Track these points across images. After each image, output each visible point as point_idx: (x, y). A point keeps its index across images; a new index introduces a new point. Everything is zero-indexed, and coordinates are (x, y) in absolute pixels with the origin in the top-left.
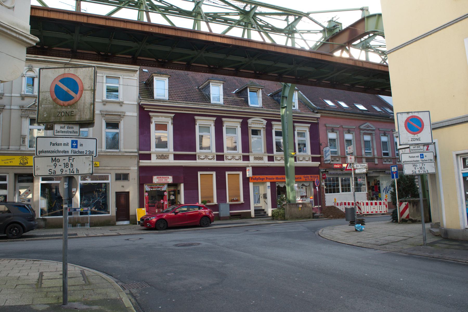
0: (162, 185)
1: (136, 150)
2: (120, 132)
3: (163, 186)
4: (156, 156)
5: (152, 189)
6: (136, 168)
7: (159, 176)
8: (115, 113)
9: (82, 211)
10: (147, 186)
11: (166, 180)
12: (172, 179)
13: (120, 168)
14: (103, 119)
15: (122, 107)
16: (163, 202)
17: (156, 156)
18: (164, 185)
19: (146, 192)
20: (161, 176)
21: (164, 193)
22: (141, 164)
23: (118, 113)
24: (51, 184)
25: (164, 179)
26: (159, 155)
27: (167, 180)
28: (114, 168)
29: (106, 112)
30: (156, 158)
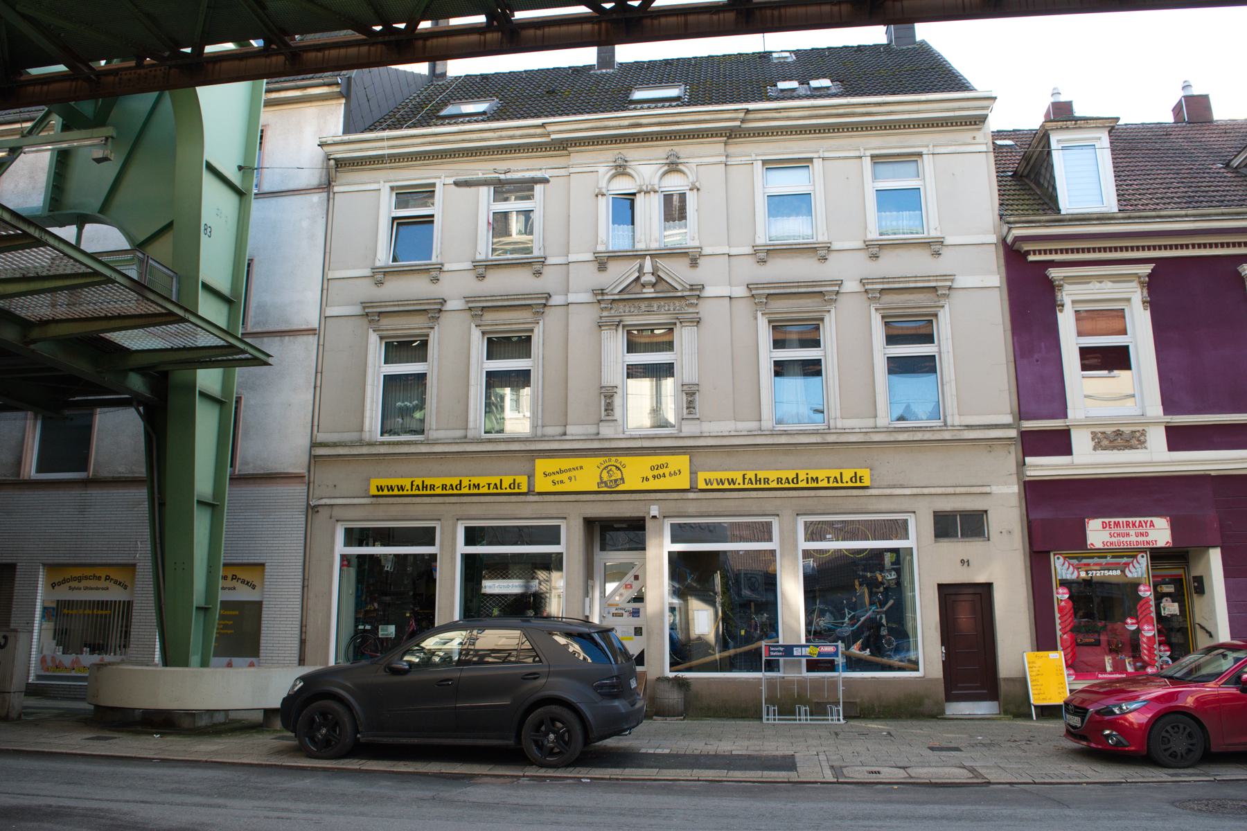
0: (1128, 557)
3: (1131, 560)
4: (1090, 436)
7: (1113, 520)
9: (815, 657)
10: (1062, 560)
11: (1142, 534)
13: (951, 490)
16: (1134, 627)
17: (1093, 439)
20: (1121, 520)
23: (929, 281)
25: (1132, 532)
26: (1103, 433)
28: (926, 491)
29: (883, 283)
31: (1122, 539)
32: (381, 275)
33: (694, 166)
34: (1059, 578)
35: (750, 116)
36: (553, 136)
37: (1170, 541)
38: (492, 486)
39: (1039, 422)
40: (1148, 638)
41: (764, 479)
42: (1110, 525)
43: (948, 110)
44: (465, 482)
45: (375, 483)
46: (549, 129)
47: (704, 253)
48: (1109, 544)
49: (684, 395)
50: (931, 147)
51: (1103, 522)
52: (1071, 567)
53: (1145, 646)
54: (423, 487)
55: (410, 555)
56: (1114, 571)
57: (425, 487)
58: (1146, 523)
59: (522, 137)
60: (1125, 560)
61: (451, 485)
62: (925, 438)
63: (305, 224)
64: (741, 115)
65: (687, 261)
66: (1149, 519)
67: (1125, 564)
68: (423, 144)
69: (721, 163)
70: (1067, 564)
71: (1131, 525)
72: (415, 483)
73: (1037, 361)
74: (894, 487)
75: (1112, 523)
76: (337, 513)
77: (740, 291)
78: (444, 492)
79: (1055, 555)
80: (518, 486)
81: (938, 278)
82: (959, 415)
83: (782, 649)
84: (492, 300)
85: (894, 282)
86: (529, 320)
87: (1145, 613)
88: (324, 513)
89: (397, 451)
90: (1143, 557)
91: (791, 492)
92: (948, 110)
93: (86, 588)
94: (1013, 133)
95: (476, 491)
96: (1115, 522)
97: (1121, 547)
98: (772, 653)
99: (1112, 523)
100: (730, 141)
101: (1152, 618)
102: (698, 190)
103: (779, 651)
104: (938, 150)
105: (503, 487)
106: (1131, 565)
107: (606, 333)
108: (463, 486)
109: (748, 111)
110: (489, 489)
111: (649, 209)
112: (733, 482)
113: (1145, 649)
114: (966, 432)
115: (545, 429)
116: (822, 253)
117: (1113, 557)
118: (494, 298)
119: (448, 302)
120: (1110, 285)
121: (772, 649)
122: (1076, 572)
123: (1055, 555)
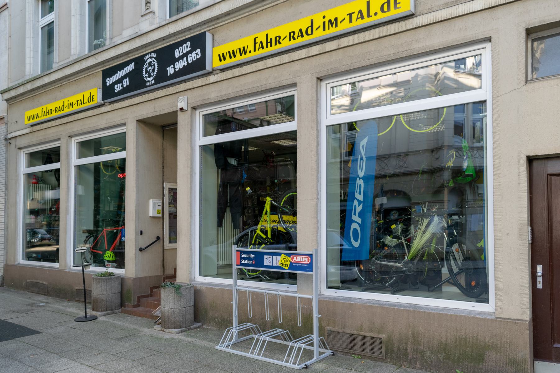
38: (354, 16)
41: (276, 38)
45: (28, 114)
54: (267, 43)
55: (234, 131)
57: (269, 42)
61: (301, 30)
72: (258, 41)
83: (252, 256)
91: (310, 49)
103: (250, 259)
108: (315, 27)
110: (351, 21)
121: (243, 256)
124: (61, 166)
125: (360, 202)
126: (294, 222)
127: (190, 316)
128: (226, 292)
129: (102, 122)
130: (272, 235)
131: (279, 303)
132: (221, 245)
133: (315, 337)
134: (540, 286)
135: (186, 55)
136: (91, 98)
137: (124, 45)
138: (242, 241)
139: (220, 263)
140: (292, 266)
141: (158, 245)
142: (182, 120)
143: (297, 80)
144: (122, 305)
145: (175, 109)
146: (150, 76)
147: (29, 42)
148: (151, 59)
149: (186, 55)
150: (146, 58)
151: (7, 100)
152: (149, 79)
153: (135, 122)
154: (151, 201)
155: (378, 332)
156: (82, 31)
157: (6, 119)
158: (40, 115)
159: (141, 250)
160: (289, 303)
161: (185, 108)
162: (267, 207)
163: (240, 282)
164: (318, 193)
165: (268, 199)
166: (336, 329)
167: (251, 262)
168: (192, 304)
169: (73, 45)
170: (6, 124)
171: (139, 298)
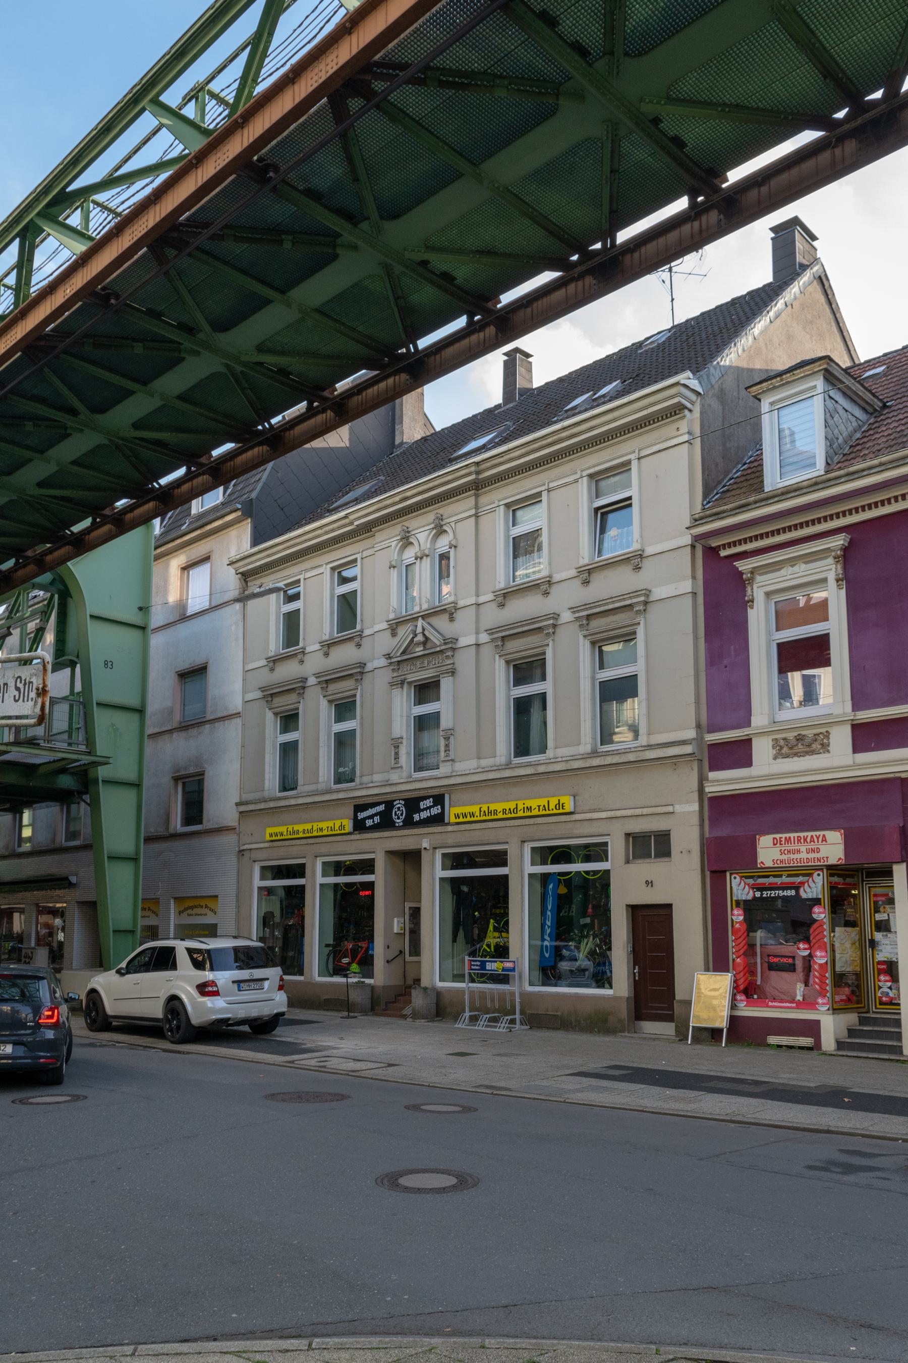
0: (804, 875)
1: (691, 734)
2: (509, 690)
3: (806, 878)
4: (771, 743)
5: (758, 894)
6: (696, 807)
7: (784, 836)
8: (613, 602)
9: (500, 972)
10: (738, 879)
11: (813, 851)
12: (842, 847)
13: (638, 812)
14: (581, 638)
15: (550, 596)
16: (806, 953)
17: (773, 748)
18: (810, 875)
19: (738, 903)
20: (792, 835)
21: (810, 912)
22: (711, 789)
23: (624, 600)
24: (274, 879)
25: (803, 849)
26: (785, 739)
27: (818, 851)
28: (618, 813)
29: (586, 609)
30: (772, 752)
31: (792, 856)
32: (275, 661)
33: (453, 524)
34: (735, 898)
35: (482, 467)
36: (356, 523)
37: (843, 857)
39: (716, 734)
40: (820, 965)
42: (781, 841)
43: (641, 409)
44: (520, 807)
45: (269, 830)
46: (352, 517)
47: (459, 606)
48: (779, 862)
49: (393, 748)
50: (496, 502)
51: (774, 838)
52: (747, 887)
53: (816, 973)
56: (789, 891)
57: (490, 813)
58: (818, 838)
59: (339, 528)
60: (800, 879)
62: (614, 761)
63: (233, 628)
64: (473, 469)
65: (446, 616)
66: (821, 833)
67: (800, 883)
68: (284, 549)
69: (470, 516)
70: (743, 883)
71: (802, 841)
73: (726, 667)
74: (594, 811)
75: (783, 840)
76: (255, 855)
77: (484, 638)
78: (505, 816)
79: (731, 874)
80: (563, 806)
81: (631, 595)
82: (579, 744)
83: (479, 963)
84: (287, 685)
85: (595, 607)
86: (352, 687)
87: (817, 938)
88: (247, 854)
89: (279, 805)
90: (819, 875)
92: (641, 409)
93: (197, 915)
94: (885, 358)
95: (529, 814)
96: (786, 838)
97: (791, 865)
98: (473, 967)
99: (783, 840)
100: (480, 491)
101: (825, 943)
102: (455, 547)
103: (477, 965)
104: (643, 453)
105: (550, 809)
106: (806, 885)
107: (396, 692)
108: (519, 809)
109: (477, 464)
111: (424, 572)
112: (282, 834)
113: (817, 977)
114: (647, 752)
115: (558, 750)
116: (544, 587)
117: (789, 876)
118: (587, 606)
119: (461, 639)
120: (803, 567)
121: (473, 963)
122: (751, 892)
123: (731, 874)
124: (306, 881)
125: (549, 927)
126: (508, 938)
127: (434, 1011)
128: (461, 992)
129: (352, 848)
130: (495, 949)
131: (496, 997)
132: (455, 960)
133: (518, 1016)
134: (637, 978)
135: (429, 808)
136: (342, 827)
137: (375, 788)
138: (473, 954)
139: (455, 972)
140: (503, 970)
141: (400, 958)
142: (425, 857)
143: (508, 840)
144: (373, 1009)
145: (419, 847)
146: (398, 818)
147: (268, 757)
148: (399, 804)
149: (429, 808)
150: (395, 803)
151: (241, 813)
152: (398, 821)
153: (384, 853)
154: (396, 920)
155: (557, 1011)
156: (329, 760)
157: (237, 829)
158: (285, 833)
159: (388, 962)
160: (502, 996)
161: (428, 848)
162: (491, 928)
163: (471, 985)
164: (522, 920)
165: (492, 921)
166: (533, 1012)
167: (477, 968)
168: (435, 1001)
169: (321, 774)
170: (239, 835)
171: (386, 1003)
